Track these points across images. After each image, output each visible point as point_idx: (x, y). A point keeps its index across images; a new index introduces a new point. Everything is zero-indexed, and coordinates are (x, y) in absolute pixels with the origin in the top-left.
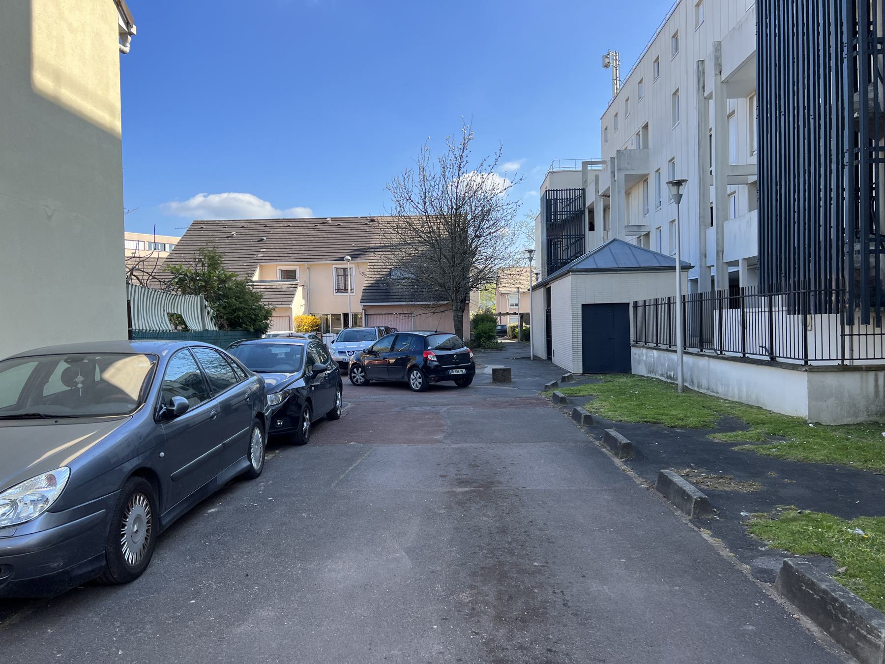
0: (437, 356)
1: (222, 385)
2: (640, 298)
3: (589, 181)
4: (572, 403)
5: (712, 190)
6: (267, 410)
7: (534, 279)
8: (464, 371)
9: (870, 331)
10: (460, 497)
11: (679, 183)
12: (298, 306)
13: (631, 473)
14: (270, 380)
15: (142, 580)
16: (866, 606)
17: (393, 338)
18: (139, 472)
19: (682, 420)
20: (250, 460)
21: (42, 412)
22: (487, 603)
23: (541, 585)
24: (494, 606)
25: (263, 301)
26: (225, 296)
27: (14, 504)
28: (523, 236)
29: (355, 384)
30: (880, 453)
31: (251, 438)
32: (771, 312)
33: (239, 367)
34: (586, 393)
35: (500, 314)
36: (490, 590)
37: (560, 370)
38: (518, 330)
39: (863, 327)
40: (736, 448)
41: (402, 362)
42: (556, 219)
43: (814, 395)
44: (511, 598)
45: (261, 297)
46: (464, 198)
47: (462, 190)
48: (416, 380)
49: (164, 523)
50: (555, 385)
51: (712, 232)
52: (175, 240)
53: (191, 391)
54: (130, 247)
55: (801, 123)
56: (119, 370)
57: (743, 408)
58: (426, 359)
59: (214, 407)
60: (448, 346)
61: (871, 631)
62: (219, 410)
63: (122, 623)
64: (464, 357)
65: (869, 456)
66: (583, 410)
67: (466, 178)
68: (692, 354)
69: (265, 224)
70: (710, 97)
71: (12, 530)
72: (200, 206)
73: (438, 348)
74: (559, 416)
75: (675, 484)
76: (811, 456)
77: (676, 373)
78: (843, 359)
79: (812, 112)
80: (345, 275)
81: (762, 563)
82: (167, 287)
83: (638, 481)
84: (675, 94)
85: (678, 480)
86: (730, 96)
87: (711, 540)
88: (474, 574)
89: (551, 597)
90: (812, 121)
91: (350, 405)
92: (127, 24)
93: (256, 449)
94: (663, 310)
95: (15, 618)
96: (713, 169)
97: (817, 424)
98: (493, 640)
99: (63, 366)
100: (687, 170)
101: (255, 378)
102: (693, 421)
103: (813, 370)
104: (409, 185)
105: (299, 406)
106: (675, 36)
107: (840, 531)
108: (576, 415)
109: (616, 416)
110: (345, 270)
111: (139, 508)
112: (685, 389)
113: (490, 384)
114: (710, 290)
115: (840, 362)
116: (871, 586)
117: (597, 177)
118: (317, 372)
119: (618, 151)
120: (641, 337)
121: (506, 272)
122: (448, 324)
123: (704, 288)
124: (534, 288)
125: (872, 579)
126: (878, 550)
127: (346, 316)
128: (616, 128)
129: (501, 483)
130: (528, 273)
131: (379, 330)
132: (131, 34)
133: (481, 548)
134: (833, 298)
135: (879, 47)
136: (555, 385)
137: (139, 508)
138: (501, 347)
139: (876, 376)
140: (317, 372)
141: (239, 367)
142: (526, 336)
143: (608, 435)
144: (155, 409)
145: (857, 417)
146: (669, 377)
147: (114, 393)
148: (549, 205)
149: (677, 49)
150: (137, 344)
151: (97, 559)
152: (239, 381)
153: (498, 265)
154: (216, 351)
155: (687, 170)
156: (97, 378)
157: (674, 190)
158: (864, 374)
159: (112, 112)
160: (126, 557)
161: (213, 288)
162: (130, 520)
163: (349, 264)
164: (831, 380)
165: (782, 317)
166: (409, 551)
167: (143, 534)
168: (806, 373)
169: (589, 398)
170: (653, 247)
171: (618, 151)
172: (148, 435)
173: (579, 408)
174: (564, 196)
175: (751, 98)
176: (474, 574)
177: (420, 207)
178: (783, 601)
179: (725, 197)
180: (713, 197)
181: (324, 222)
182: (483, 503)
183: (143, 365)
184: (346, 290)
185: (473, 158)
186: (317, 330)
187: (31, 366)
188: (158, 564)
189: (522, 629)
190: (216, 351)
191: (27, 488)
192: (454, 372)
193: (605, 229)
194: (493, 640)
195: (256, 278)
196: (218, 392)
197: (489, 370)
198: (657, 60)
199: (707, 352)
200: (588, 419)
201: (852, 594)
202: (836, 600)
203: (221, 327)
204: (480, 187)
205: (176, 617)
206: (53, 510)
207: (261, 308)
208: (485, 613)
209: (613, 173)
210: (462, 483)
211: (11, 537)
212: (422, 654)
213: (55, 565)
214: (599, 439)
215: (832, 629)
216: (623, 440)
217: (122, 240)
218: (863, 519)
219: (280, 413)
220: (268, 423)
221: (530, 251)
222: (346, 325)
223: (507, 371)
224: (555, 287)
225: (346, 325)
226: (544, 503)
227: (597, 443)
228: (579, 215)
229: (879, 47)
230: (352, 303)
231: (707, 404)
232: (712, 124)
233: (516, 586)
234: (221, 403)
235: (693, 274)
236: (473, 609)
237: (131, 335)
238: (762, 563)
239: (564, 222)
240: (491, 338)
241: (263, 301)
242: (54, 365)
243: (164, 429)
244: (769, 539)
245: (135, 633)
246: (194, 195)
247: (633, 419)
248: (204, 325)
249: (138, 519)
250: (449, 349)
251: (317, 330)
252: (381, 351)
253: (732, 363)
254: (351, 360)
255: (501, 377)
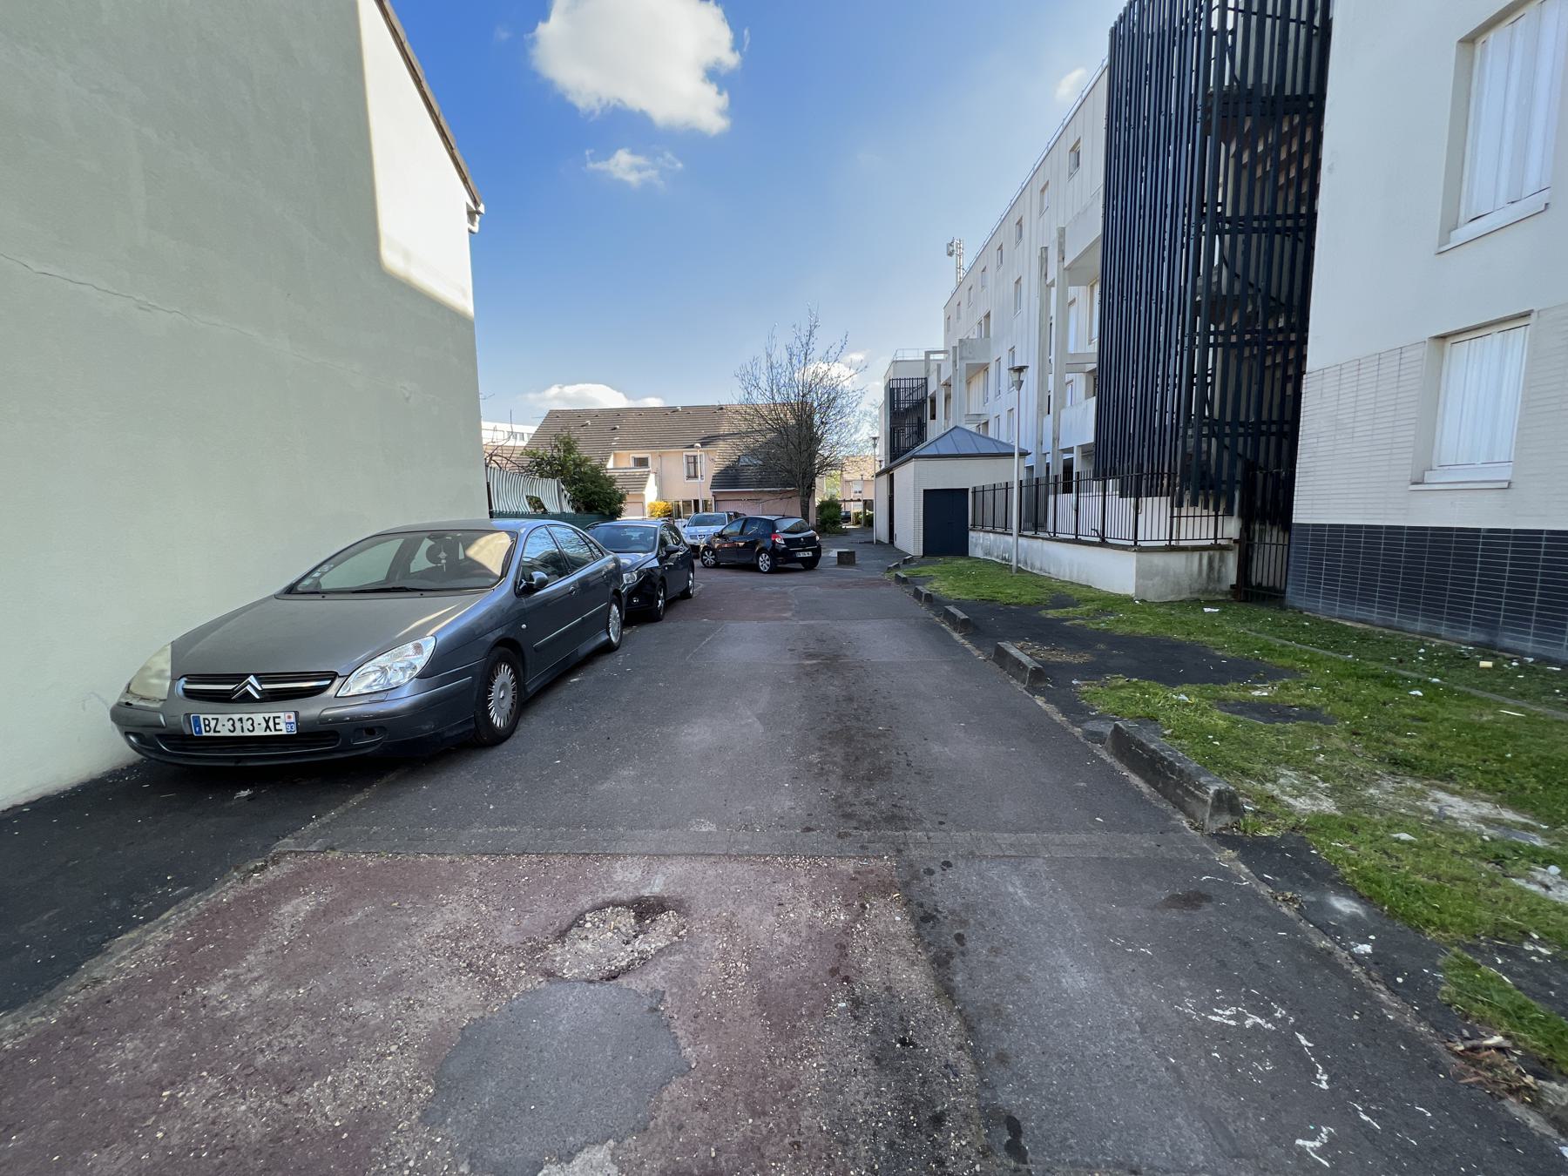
0: (785, 540)
1: (577, 564)
2: (979, 484)
3: (931, 370)
4: (913, 583)
5: (1051, 378)
6: (623, 588)
7: (877, 466)
8: (810, 554)
9: (1198, 513)
10: (808, 669)
11: (1020, 370)
12: (651, 493)
13: (969, 646)
14: (626, 560)
15: (510, 742)
16: (1195, 765)
17: (741, 523)
18: (502, 642)
19: (1017, 598)
20: (609, 634)
21: (408, 586)
22: (835, 764)
23: (886, 747)
24: (842, 767)
25: (618, 485)
26: (580, 480)
27: (383, 670)
28: (868, 424)
29: (706, 566)
30: (1202, 627)
31: (609, 613)
32: (1104, 496)
33: (596, 547)
34: (926, 574)
35: (845, 501)
36: (838, 752)
37: (901, 553)
38: (861, 516)
39: (1191, 509)
40: (1067, 623)
41: (751, 545)
42: (899, 408)
43: (1141, 574)
44: (857, 759)
45: (615, 481)
46: (810, 385)
47: (808, 378)
48: (764, 561)
49: (529, 690)
50: (897, 567)
51: (1049, 420)
52: (533, 429)
53: (550, 569)
54: (487, 437)
55: (1143, 308)
56: (482, 548)
57: (1074, 587)
58: (774, 542)
59: (572, 583)
60: (796, 529)
61: (1199, 787)
62: (577, 585)
63: (493, 781)
64: (811, 540)
65: (1192, 630)
66: (924, 589)
67: (811, 368)
68: (1026, 536)
69: (618, 413)
70: (1052, 284)
71: (382, 696)
72: (556, 398)
73: (784, 532)
74: (902, 595)
75: (1011, 655)
76: (1137, 629)
77: (1011, 555)
78: (1171, 540)
79: (1154, 297)
80: (695, 463)
81: (1092, 726)
82: (528, 471)
83: (976, 653)
84: (1017, 282)
85: (1014, 651)
86: (1071, 284)
87: (1045, 706)
88: (822, 738)
89: (895, 758)
90: (1154, 306)
91: (702, 585)
92: (475, 202)
93: (614, 625)
94: (1000, 495)
95: (392, 776)
96: (1052, 357)
97: (1142, 601)
98: (841, 797)
99: (427, 543)
100: (1027, 355)
101: (611, 557)
102: (1027, 599)
103: (1142, 550)
104: (757, 373)
105: (654, 585)
106: (1019, 223)
107: (1165, 697)
108: (918, 594)
109: (956, 595)
110: (695, 457)
111: (504, 675)
112: (1019, 570)
113: (836, 566)
114: (1044, 475)
115: (1167, 543)
116: (1196, 747)
117: (939, 366)
118: (670, 553)
119: (961, 341)
120: (979, 521)
121: (851, 459)
122: (795, 507)
123: (1039, 473)
124: (878, 475)
125: (1197, 740)
126: (1202, 715)
127: (696, 502)
128: (958, 318)
129: (845, 656)
130: (872, 460)
131: (729, 515)
132: (479, 213)
133: (829, 715)
134: (1165, 482)
135: (1227, 226)
136: (897, 567)
137: (504, 675)
138: (846, 532)
139: (1201, 556)
140: (670, 553)
141: (596, 547)
142: (869, 521)
143: (947, 611)
144: (516, 583)
145: (1180, 594)
146: (1004, 559)
147: (476, 569)
148: (892, 394)
149: (1021, 236)
150: (497, 522)
151: (468, 722)
152: (596, 559)
153: (842, 453)
154: (575, 531)
155: (1027, 355)
156: (461, 557)
157: (1015, 376)
158: (1189, 554)
159: (464, 295)
160: (494, 721)
161: (569, 472)
162: (495, 688)
163: (698, 452)
164: (1159, 560)
165: (1114, 500)
166: (760, 717)
167: (508, 700)
168: (1135, 554)
169: (929, 579)
170: (991, 434)
171: (961, 341)
172: (511, 608)
173: (920, 588)
174: (902, 386)
175: (1092, 286)
176: (822, 738)
177: (768, 394)
178: (1113, 760)
179: (1062, 386)
180: (1051, 386)
181: (674, 410)
182: (830, 674)
183: (504, 541)
184: (696, 477)
185: (818, 349)
186: (669, 516)
187: (396, 544)
188: (524, 728)
189: (869, 787)
190: (573, 529)
191: (396, 656)
192: (802, 555)
193: (945, 418)
194: (841, 797)
195: (610, 465)
196: (576, 569)
197: (834, 553)
198: (1000, 248)
199: (1041, 534)
200: (929, 598)
201: (1180, 754)
202: (1165, 759)
203: (578, 510)
204: (826, 374)
205: (543, 776)
206: (420, 676)
207: (615, 492)
208: (834, 772)
209: (955, 362)
210: (810, 656)
211: (383, 701)
212: (775, 809)
213: (427, 727)
214: (939, 616)
215: (1160, 785)
216: (962, 615)
217: (479, 430)
218: (1187, 687)
219: (636, 590)
220: (624, 601)
221: (875, 439)
222: (697, 510)
223: (852, 554)
224: (896, 472)
225: (697, 510)
226: (889, 674)
227: (937, 619)
228: (921, 403)
229: (1227, 226)
230: (701, 489)
231: (1040, 583)
232: (1053, 313)
233: (862, 748)
234: (579, 579)
235: (1030, 461)
236: (822, 769)
237: (492, 515)
238: (1092, 726)
239: (907, 410)
240: (836, 523)
241: (618, 485)
242: (419, 542)
243: (525, 602)
244: (1099, 705)
245: (506, 789)
246: (550, 386)
247: (972, 597)
248: (561, 509)
249: (503, 686)
250: (797, 533)
251: (669, 516)
252: (731, 535)
253: (1065, 544)
254: (702, 543)
255: (846, 559)
